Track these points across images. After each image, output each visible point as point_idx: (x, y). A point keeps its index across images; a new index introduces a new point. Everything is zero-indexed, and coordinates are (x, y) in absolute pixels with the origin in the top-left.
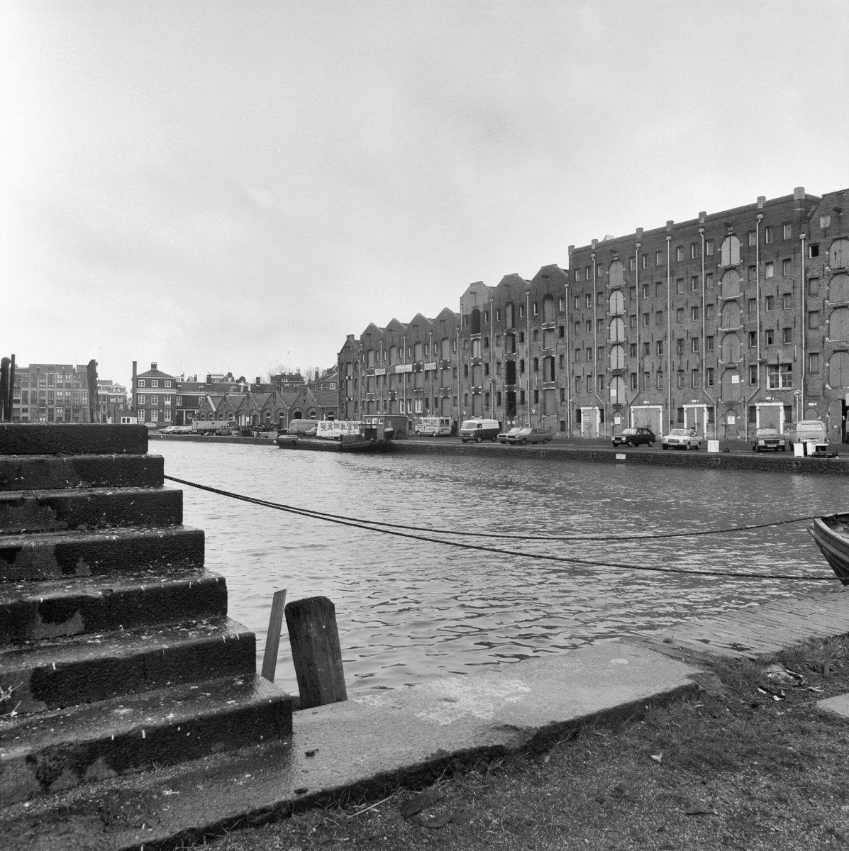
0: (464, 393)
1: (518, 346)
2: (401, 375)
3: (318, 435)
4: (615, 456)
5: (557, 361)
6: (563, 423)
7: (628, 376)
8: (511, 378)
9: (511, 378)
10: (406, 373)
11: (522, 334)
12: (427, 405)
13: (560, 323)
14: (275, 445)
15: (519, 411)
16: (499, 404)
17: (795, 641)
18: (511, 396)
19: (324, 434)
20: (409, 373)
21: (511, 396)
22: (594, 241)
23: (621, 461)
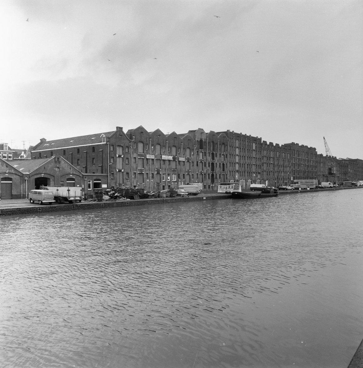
0: (197, 173)
1: (215, 158)
2: (164, 160)
3: (218, 192)
4: (203, 198)
5: (225, 165)
6: (205, 186)
7: (239, 172)
8: (213, 169)
9: (213, 169)
10: (168, 160)
11: (216, 154)
12: (179, 177)
13: (226, 153)
14: (299, 193)
15: (215, 181)
16: (209, 178)
17: (121, 320)
18: (213, 175)
19: (221, 192)
20: (169, 161)
21: (213, 175)
22: (246, 134)
23: (205, 200)
